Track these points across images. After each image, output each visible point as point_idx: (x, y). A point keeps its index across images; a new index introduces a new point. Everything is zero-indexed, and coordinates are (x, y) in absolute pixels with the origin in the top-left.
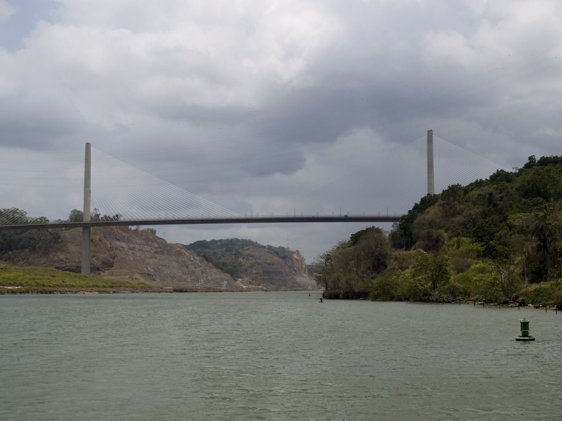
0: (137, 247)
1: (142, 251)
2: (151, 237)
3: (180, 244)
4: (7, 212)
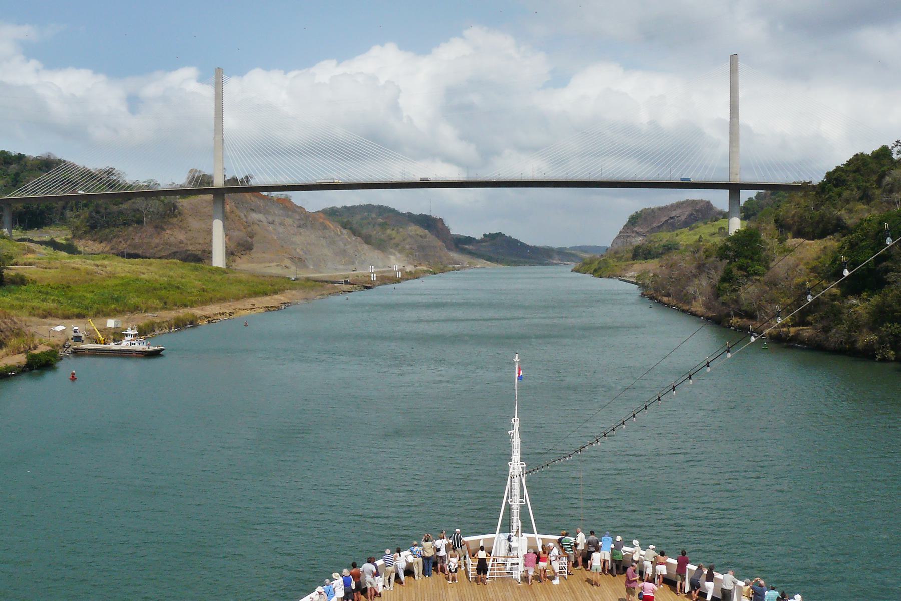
0: (278, 220)
1: (284, 225)
2: (288, 207)
3: (319, 211)
4: (100, 172)
